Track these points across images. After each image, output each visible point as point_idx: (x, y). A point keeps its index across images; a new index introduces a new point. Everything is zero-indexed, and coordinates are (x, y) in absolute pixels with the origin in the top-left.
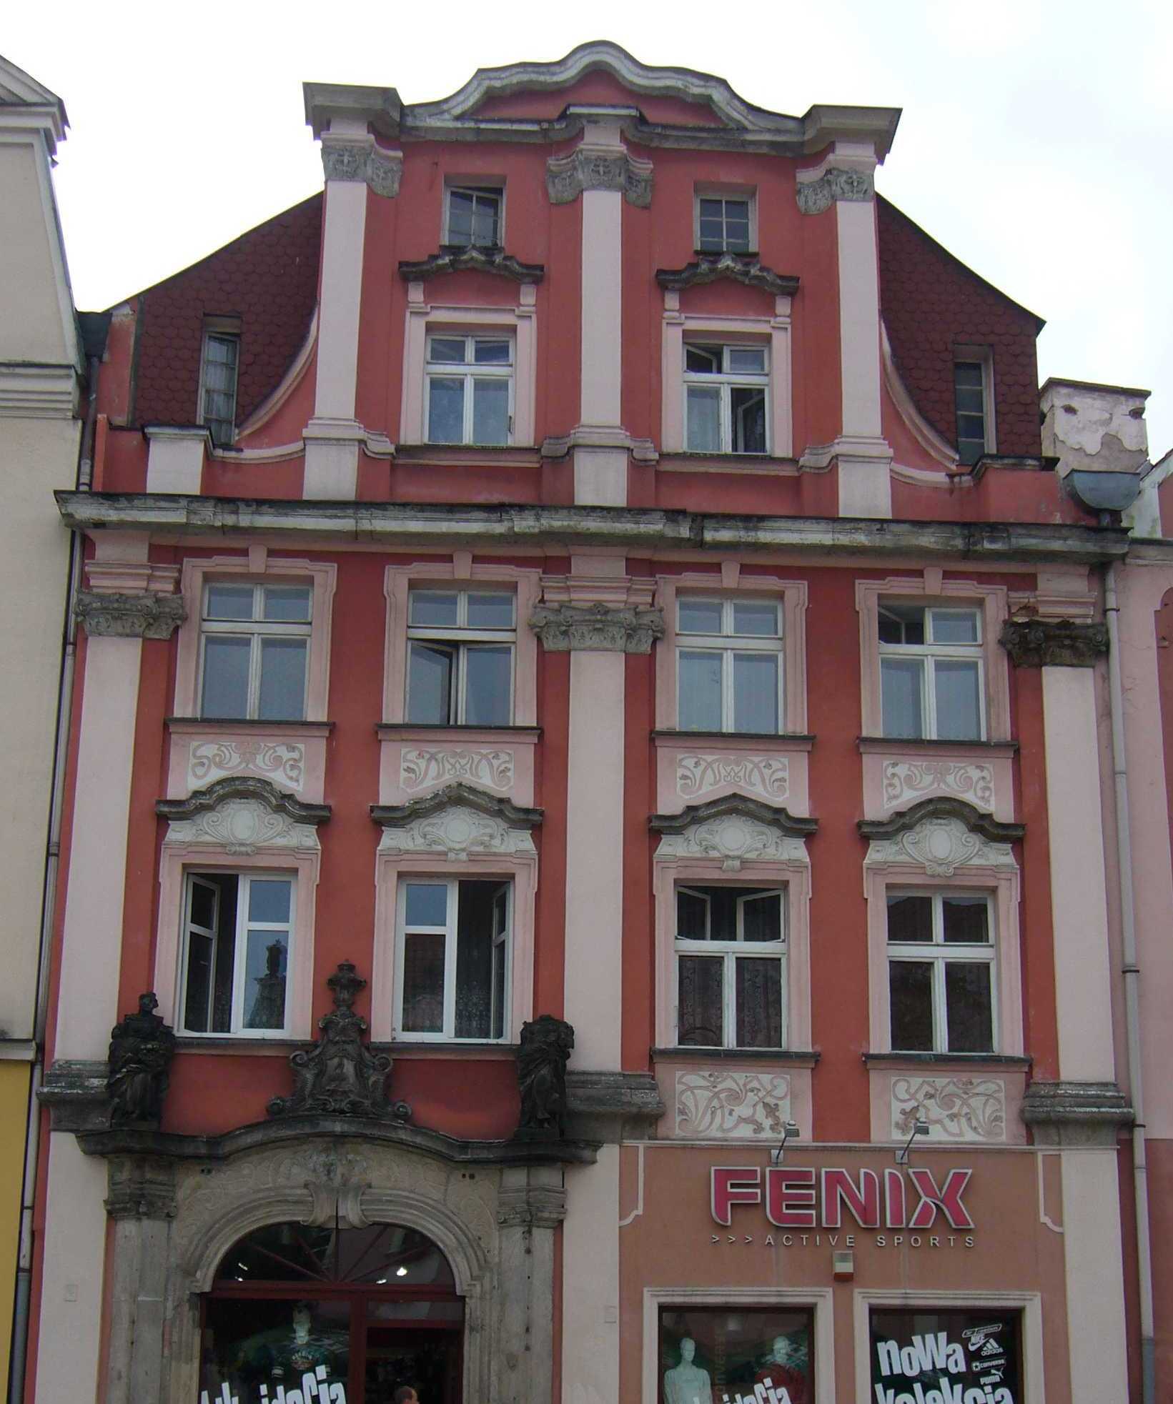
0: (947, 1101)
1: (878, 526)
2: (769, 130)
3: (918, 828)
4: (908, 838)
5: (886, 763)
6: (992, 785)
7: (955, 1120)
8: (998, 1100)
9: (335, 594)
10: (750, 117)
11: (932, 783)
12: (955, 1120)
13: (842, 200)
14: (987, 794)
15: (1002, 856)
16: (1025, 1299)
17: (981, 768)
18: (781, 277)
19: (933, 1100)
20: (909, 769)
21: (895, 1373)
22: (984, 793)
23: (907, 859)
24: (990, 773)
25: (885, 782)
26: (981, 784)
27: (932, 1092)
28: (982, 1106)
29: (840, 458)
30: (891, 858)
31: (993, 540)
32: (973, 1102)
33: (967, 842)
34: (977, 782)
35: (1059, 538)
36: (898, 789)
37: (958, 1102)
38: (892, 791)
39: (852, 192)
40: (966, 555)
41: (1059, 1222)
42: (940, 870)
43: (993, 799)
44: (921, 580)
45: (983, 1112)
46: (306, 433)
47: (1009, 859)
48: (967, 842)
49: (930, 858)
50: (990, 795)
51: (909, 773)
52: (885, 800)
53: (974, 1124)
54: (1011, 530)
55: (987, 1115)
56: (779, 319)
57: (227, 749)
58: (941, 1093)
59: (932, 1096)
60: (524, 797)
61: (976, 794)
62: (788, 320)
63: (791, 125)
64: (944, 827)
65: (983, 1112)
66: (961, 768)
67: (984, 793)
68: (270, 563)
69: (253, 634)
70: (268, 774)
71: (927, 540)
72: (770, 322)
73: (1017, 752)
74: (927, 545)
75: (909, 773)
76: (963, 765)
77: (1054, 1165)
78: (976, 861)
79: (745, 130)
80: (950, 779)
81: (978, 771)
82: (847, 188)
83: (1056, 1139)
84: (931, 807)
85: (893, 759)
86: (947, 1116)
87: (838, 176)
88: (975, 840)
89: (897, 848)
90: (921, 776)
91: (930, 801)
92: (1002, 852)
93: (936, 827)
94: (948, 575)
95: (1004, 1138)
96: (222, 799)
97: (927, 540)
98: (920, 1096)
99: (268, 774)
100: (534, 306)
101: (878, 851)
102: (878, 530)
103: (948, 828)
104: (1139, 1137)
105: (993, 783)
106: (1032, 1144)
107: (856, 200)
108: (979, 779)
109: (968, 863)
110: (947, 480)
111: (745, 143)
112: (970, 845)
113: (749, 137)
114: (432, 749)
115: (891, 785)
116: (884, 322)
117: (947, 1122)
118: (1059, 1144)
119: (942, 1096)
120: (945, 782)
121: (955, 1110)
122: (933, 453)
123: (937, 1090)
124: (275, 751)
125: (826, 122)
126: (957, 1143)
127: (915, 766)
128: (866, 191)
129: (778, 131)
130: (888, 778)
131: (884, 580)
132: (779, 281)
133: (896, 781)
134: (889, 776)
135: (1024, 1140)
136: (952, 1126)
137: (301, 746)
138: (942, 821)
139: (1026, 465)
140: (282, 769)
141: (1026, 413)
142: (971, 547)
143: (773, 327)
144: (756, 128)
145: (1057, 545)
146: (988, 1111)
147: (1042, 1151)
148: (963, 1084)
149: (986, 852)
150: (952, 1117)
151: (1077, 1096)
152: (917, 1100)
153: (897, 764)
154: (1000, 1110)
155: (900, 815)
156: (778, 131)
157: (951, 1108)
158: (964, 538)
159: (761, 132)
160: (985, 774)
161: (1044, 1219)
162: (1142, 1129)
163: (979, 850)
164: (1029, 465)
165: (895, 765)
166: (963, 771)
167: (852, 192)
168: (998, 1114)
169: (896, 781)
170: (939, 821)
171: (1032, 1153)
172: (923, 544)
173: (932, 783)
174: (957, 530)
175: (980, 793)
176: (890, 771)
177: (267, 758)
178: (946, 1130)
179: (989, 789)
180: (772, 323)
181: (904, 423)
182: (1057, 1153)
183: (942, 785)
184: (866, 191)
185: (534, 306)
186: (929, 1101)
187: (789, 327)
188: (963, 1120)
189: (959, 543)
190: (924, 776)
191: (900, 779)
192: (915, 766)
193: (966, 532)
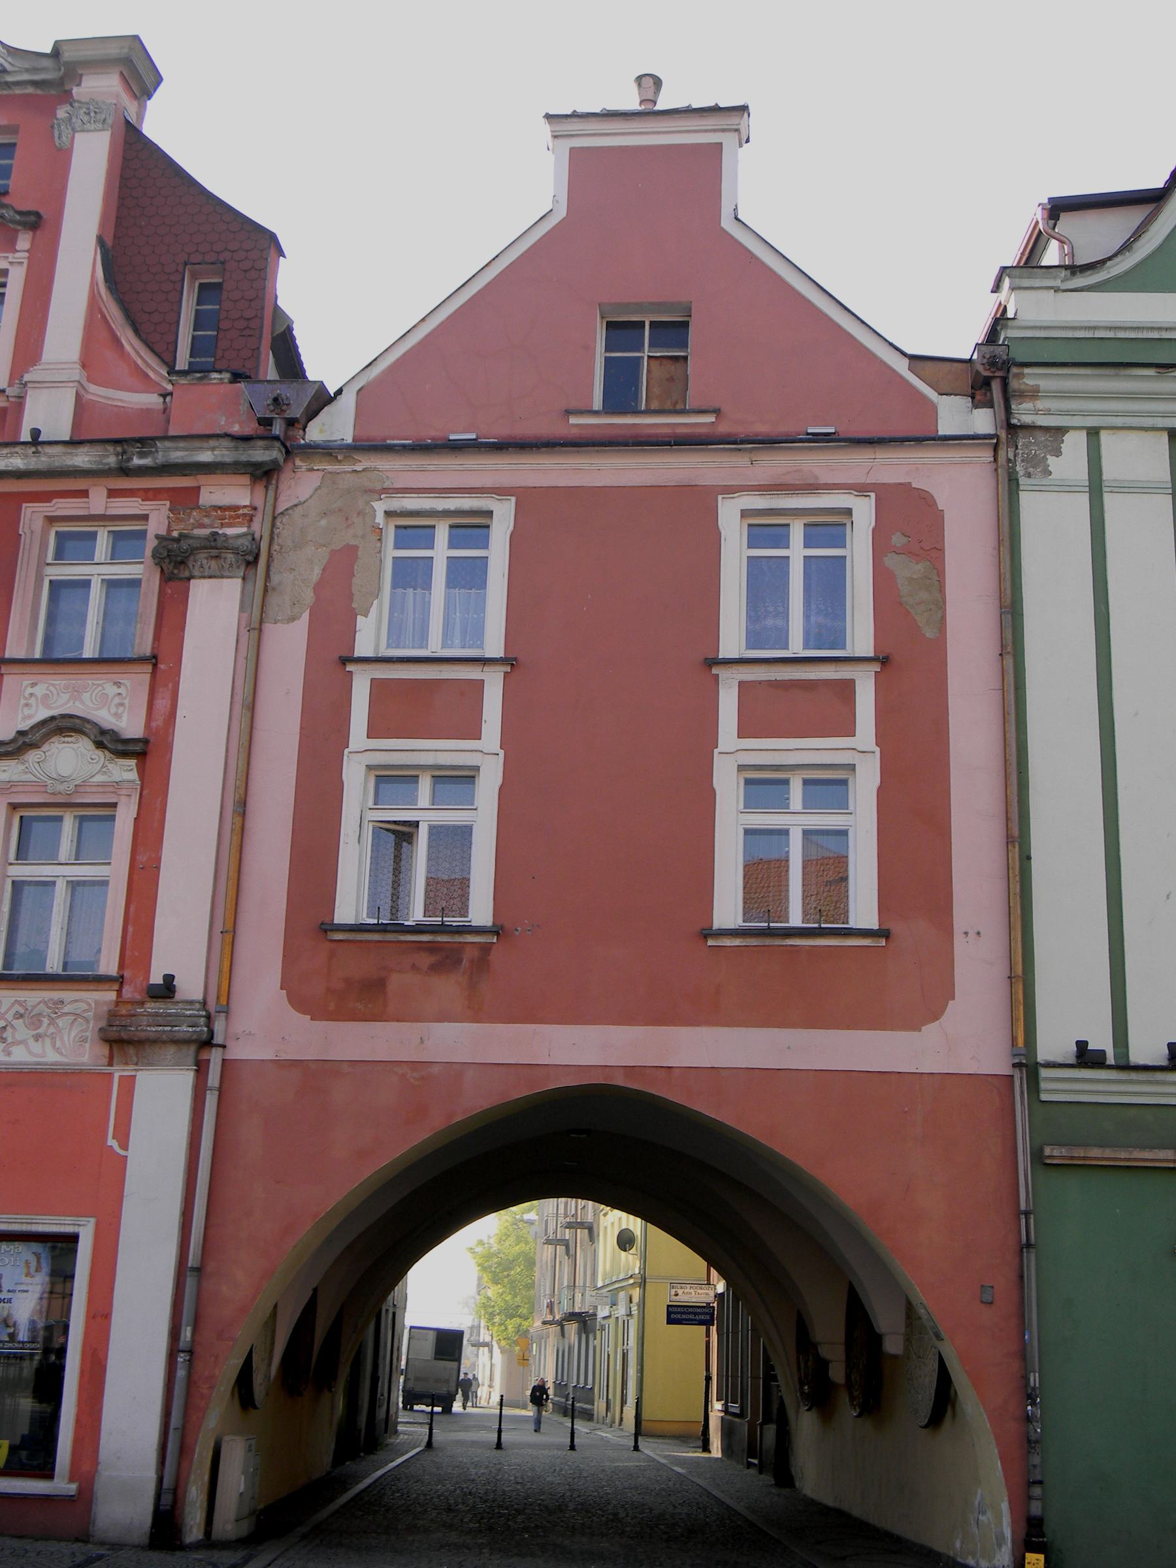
0: (35, 1021)
1: (33, 449)
2: (27, 70)
3: (45, 747)
4: (32, 756)
5: (25, 683)
6: (126, 702)
7: (40, 1039)
8: (87, 1021)
9: (874, 530)
10: (10, 59)
11: (68, 701)
12: (40, 1039)
13: (83, 131)
14: (121, 709)
15: (125, 771)
16: (79, 1225)
17: (118, 684)
18: (20, 213)
19: (21, 1020)
20: (47, 689)
21: (705, 1327)
22: (117, 709)
23: (30, 777)
24: (127, 690)
25: (23, 702)
26: (117, 700)
27: (22, 1011)
28: (68, 1027)
29: (29, 385)
30: (15, 778)
31: (142, 455)
32: (60, 1022)
33: (92, 759)
34: (112, 699)
35: (208, 449)
36: (34, 708)
37: (46, 1021)
38: (27, 711)
39: (90, 122)
40: (124, 471)
41: (125, 1146)
42: (61, 788)
43: (125, 717)
44: (86, 500)
45: (69, 1035)
46: (27, 378)
47: (133, 775)
48: (92, 759)
49: (54, 776)
50: (123, 712)
51: (48, 692)
52: (20, 719)
53: (58, 1044)
54: (158, 444)
55: (71, 1039)
56: (18, 255)
57: (56, 688)
58: (30, 1013)
59: (22, 1016)
60: (131, 725)
61: (109, 711)
62: (26, 255)
63: (46, 63)
64: (71, 745)
65: (69, 1035)
66: (99, 685)
67: (117, 709)
68: (109, 505)
69: (93, 575)
70: (95, 712)
71: (82, 458)
72: (7, 257)
73: (155, 666)
74: (81, 465)
75: (48, 692)
76: (101, 682)
77: (128, 1085)
78: (99, 778)
79: (5, 71)
80: (86, 696)
81: (115, 687)
82: (86, 118)
83: (135, 1059)
84: (53, 725)
85: (35, 678)
86: (33, 1036)
87: (80, 108)
88: (99, 755)
89: (23, 767)
90: (58, 694)
91: (53, 718)
92: (126, 768)
93: (64, 745)
94: (113, 493)
95: (86, 1059)
96: (46, 737)
97: (82, 458)
98: (9, 1016)
99: (95, 712)
100: (27, 251)
101: (5, 770)
102: (33, 453)
103: (75, 746)
104: (215, 1057)
105: (128, 698)
106: (112, 1066)
107: (95, 130)
108: (115, 696)
109: (91, 780)
110: (161, 400)
111: (8, 85)
112: (95, 761)
113: (10, 79)
114: (117, 677)
115: (27, 705)
116: (101, 249)
117: (31, 1042)
118: (136, 1064)
119: (32, 1015)
120: (82, 702)
121: (40, 1031)
122: (151, 374)
123: (27, 1009)
124: (104, 689)
125: (67, 55)
126: (38, 1064)
127: (53, 685)
128: (105, 120)
129: (35, 70)
130: (25, 698)
131: (50, 502)
132: (18, 217)
133: (32, 701)
134: (26, 695)
135: (105, 1061)
136: (36, 1047)
137: (127, 683)
138: (69, 739)
139: (211, 379)
140: (107, 707)
141: (248, 327)
142: (123, 463)
143: (11, 263)
144: (17, 69)
145: (206, 457)
146: (73, 1034)
147: (119, 1072)
148: (54, 1004)
149: (111, 769)
150: (37, 1038)
151: (157, 1015)
152: (6, 1020)
153: (36, 684)
154: (86, 1030)
155: (21, 733)
156: (35, 70)
157: (39, 1028)
158: (117, 455)
159: (20, 72)
160: (122, 690)
161: (112, 1142)
162: (220, 1050)
163: (103, 767)
164: (215, 378)
165: (33, 685)
166: (100, 688)
167: (90, 122)
168: (84, 1034)
169: (32, 701)
170: (66, 739)
171: (110, 1073)
172: (76, 464)
173: (68, 701)
174: (110, 448)
175: (113, 710)
176: (29, 690)
177: (93, 696)
178: (30, 1053)
179: (122, 704)
180: (10, 260)
181: (122, 346)
182: (133, 1073)
183: (77, 704)
184: (105, 120)
185: (27, 251)
186: (17, 1021)
187: (26, 261)
188: (48, 1041)
189: (112, 460)
190: (61, 694)
191: (37, 699)
192: (53, 685)
193: (119, 449)
